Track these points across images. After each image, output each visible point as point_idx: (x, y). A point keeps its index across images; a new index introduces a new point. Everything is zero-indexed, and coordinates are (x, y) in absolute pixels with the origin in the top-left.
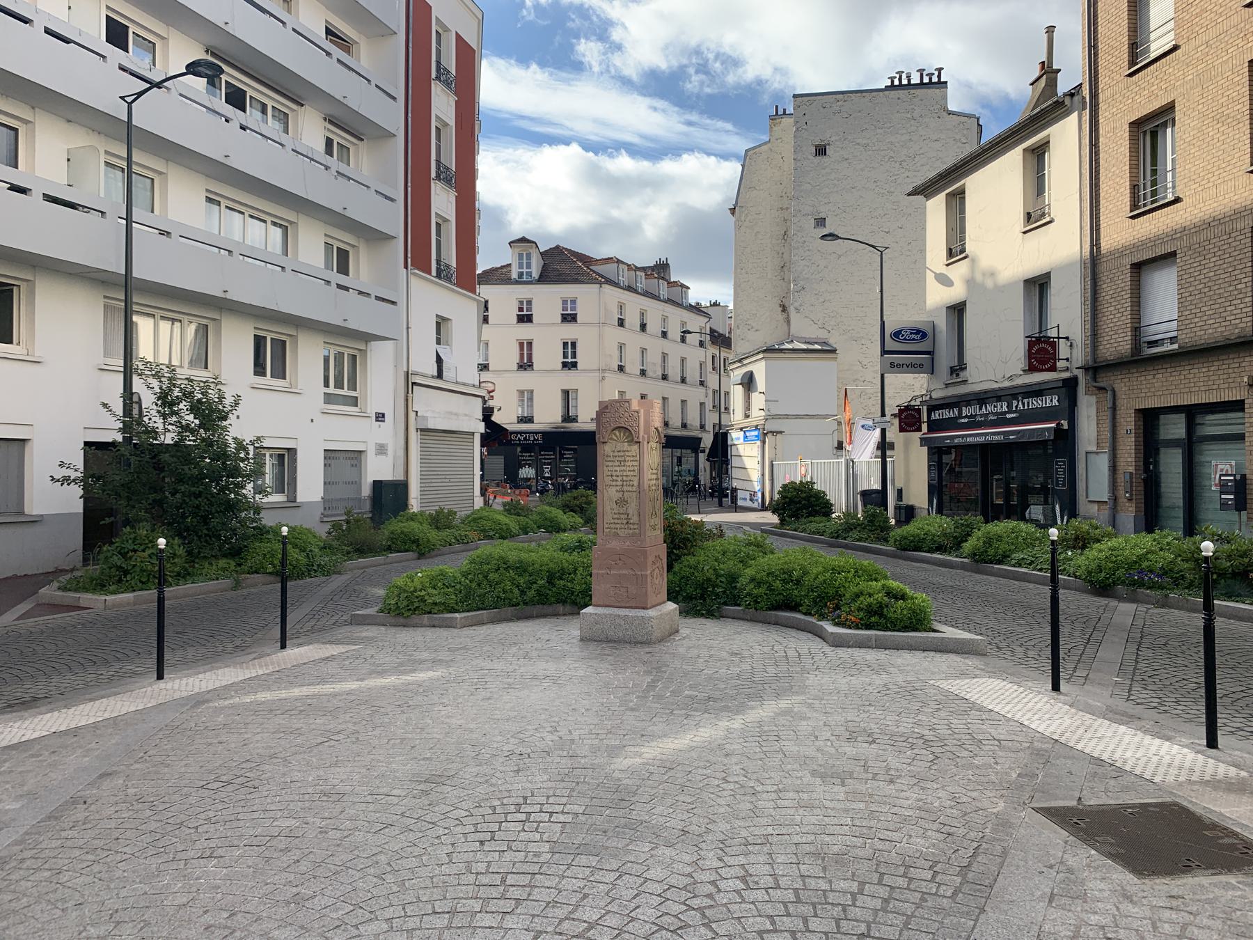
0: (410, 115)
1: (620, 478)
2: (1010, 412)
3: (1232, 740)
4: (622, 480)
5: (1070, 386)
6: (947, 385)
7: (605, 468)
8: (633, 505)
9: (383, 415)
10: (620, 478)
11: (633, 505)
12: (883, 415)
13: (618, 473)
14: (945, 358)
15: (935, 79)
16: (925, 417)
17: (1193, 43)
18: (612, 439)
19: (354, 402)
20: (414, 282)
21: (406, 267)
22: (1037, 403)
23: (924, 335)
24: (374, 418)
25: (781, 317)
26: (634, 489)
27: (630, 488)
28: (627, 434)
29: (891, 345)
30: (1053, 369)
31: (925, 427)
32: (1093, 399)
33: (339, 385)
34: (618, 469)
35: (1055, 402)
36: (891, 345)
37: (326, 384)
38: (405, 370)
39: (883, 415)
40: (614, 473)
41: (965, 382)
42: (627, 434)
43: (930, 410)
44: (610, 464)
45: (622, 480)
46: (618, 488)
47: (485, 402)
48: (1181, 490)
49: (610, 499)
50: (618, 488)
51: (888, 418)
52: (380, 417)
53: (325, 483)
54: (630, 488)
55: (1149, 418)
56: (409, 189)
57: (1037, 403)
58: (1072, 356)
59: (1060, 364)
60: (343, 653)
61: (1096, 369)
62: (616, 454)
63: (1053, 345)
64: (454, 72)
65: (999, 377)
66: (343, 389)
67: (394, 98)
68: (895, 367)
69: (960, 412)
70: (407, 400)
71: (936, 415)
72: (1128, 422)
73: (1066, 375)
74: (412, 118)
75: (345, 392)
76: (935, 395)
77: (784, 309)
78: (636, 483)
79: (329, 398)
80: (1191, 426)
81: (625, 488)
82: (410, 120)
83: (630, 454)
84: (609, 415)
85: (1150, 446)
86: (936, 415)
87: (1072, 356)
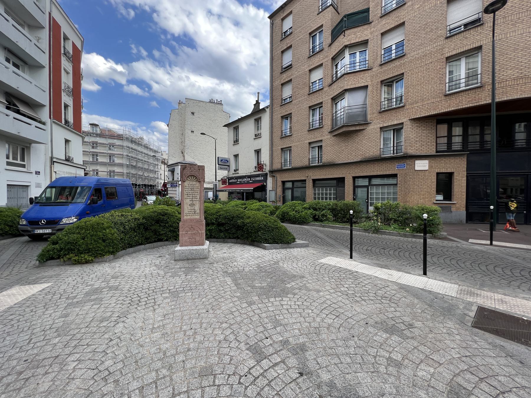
0: (51, 62)
1: (191, 196)
2: (251, 180)
3: (430, 273)
4: (192, 196)
5: (266, 174)
6: (233, 174)
7: (184, 191)
8: (197, 206)
9: (39, 172)
10: (191, 196)
11: (197, 206)
12: (216, 180)
13: (190, 194)
14: (233, 167)
15: (220, 103)
16: (227, 182)
17: (296, 101)
18: (188, 180)
19: (24, 166)
20: (54, 126)
21: (50, 118)
22: (258, 179)
23: (228, 161)
24: (34, 173)
25: (182, 155)
26: (198, 200)
27: (196, 200)
28: (194, 178)
29: (220, 163)
30: (262, 171)
31: (227, 184)
32: (271, 178)
33: (15, 158)
34: (191, 192)
35: (262, 179)
36: (220, 163)
37: (8, 157)
38: (50, 156)
39: (216, 180)
40: (189, 194)
41: (238, 173)
42: (194, 178)
43: (229, 180)
44: (187, 190)
45: (192, 196)
46: (191, 199)
47: (85, 171)
48: (465, 200)
49: (187, 204)
50: (191, 199)
51: (217, 181)
52: (38, 173)
53: (8, 198)
54: (196, 200)
55: (284, 183)
56: (52, 90)
57: (258, 179)
58: (267, 169)
59: (264, 170)
60: (40, 291)
61: (272, 172)
62: (189, 186)
63: (263, 165)
64: (71, 53)
65: (247, 172)
66: (17, 160)
67: (44, 53)
68: (221, 169)
69: (237, 180)
70: (51, 167)
71: (231, 181)
72: (280, 184)
73: (265, 173)
74: (52, 63)
75: (19, 162)
76: (230, 176)
77: (182, 153)
78: (198, 198)
79: (8, 164)
80: (293, 185)
81: (194, 200)
82: (51, 64)
83: (196, 186)
84: (187, 170)
85: (284, 190)
86: (231, 181)
87: (267, 169)
